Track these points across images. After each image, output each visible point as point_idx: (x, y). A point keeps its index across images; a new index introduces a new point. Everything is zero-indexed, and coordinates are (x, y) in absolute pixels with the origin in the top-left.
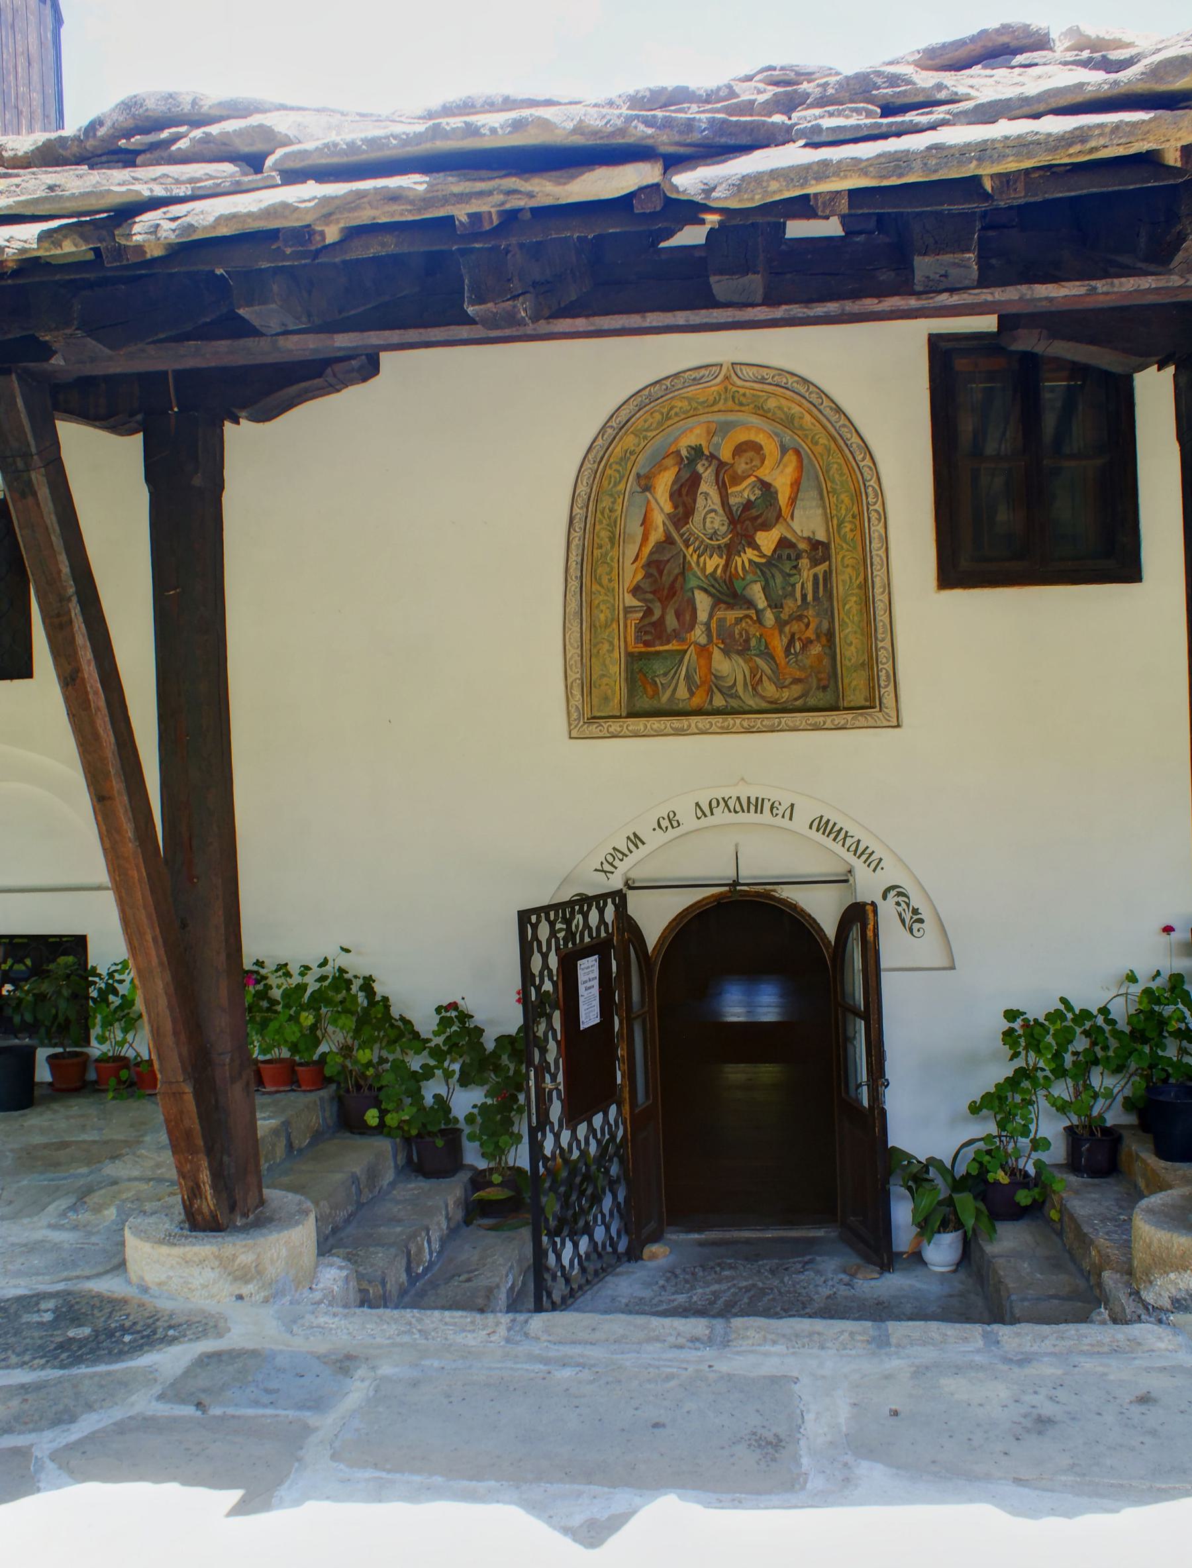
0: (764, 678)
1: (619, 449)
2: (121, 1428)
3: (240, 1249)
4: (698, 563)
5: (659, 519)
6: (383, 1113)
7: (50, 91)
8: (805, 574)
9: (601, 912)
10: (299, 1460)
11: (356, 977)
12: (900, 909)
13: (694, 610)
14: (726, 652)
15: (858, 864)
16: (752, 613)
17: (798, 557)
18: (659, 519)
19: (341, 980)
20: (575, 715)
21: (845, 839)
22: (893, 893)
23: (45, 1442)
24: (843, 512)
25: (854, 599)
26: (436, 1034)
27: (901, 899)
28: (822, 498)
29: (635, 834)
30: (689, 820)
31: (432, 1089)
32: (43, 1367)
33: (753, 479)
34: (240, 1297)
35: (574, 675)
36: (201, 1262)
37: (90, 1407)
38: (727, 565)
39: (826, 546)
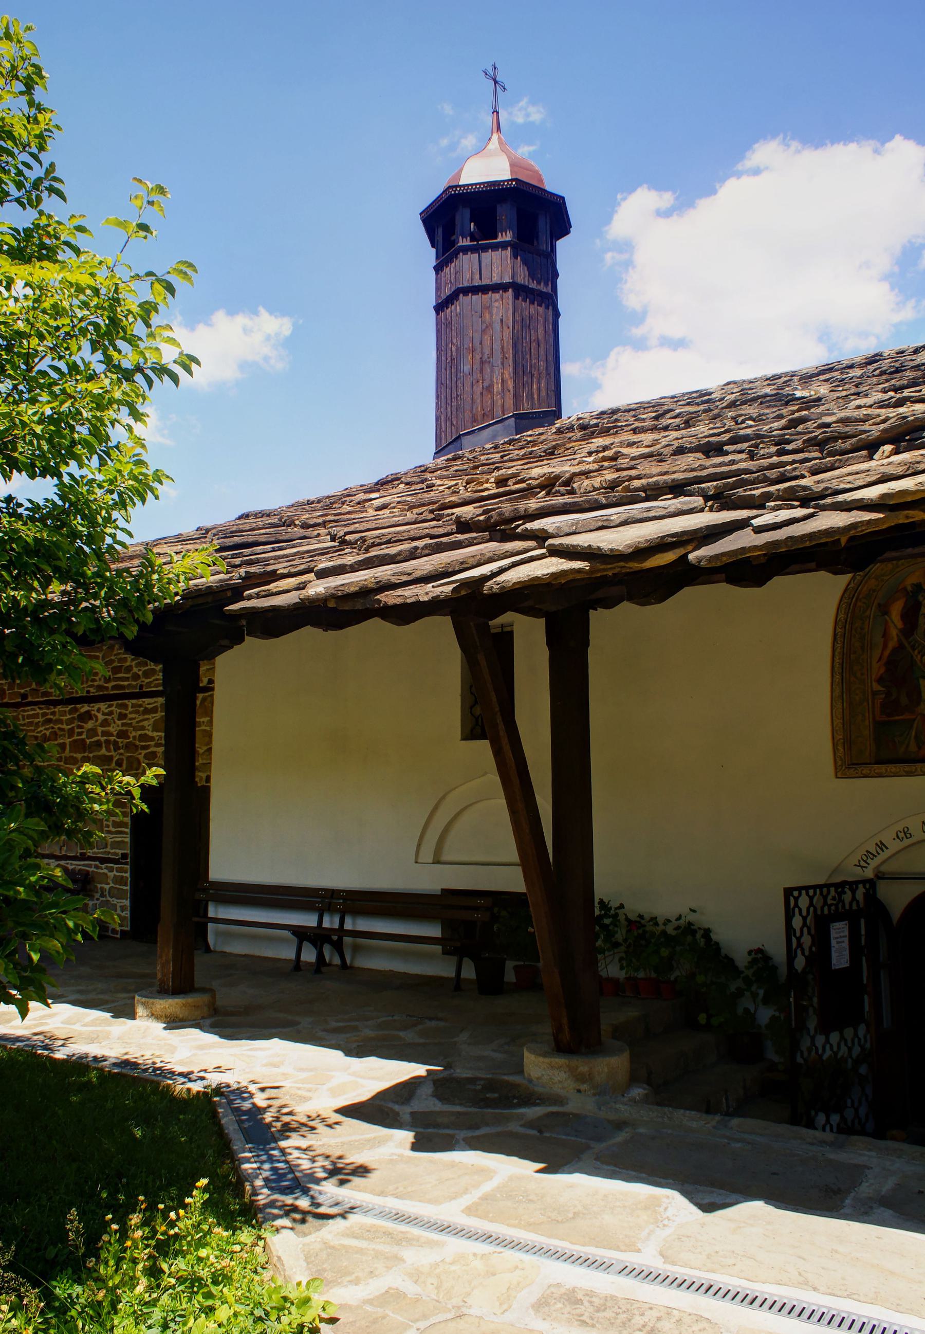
3: (582, 1065)
5: (894, 633)
7: (551, 358)
11: (700, 928)
18: (894, 633)
19: (689, 929)
20: (839, 763)
23: (462, 1134)
26: (747, 968)
31: (746, 1003)
32: (470, 1107)
34: (579, 1091)
35: (839, 737)
37: (487, 1125)
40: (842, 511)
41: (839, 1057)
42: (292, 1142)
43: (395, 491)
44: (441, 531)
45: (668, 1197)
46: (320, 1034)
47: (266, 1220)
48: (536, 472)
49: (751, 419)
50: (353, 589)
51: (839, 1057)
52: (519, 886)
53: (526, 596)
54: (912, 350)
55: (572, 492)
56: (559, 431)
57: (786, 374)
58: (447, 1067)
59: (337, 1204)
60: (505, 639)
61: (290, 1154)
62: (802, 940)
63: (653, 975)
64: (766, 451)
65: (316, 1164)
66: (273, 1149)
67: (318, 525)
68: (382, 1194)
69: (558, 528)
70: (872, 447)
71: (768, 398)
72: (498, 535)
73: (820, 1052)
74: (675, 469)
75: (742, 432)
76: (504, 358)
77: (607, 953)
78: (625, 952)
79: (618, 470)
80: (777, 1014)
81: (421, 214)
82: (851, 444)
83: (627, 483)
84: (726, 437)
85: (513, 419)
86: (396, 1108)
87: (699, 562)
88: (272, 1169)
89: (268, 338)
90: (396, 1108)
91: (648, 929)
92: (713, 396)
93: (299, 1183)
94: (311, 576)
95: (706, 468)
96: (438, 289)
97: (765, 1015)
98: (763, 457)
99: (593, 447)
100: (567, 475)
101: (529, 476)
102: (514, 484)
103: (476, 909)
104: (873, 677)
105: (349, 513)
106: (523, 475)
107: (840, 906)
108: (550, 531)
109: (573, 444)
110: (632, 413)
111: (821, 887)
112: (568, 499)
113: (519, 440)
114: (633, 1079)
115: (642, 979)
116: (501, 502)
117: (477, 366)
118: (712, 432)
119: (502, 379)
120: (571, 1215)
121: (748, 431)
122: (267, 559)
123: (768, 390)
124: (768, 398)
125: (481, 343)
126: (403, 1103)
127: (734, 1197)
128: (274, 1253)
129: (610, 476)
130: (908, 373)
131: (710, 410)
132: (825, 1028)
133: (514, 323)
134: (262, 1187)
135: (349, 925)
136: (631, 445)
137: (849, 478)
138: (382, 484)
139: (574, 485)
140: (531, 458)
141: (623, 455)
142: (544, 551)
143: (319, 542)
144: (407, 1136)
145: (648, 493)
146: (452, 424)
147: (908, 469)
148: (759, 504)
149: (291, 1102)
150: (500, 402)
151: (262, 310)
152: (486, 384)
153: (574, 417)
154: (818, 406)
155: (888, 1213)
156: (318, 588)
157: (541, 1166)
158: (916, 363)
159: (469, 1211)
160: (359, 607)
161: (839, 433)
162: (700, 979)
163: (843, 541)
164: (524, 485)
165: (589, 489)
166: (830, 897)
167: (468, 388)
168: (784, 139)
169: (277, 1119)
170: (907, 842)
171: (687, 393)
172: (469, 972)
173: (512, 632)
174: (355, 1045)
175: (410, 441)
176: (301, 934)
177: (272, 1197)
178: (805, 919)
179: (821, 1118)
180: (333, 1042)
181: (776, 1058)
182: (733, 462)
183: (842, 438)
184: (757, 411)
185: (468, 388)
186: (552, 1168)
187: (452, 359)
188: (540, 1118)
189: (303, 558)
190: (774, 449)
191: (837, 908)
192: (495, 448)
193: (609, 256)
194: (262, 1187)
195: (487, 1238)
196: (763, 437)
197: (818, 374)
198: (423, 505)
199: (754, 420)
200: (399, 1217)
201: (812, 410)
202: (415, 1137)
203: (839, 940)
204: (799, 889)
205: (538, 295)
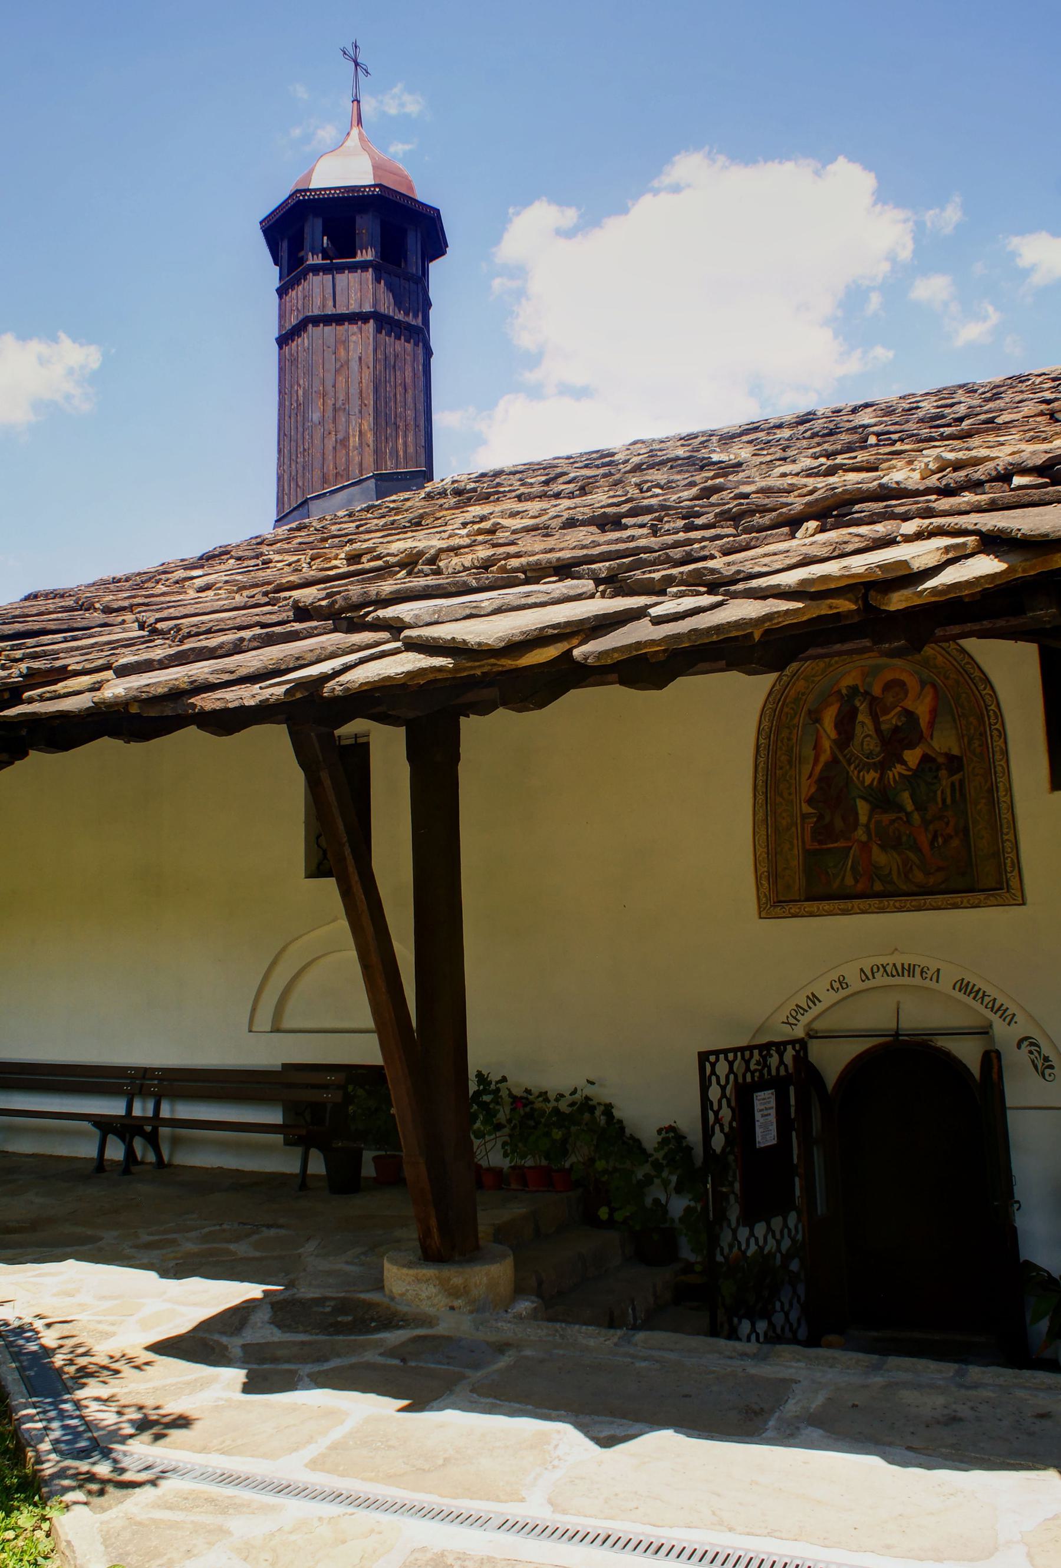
0: (914, 867)
1: (793, 691)
2: (352, 1367)
3: (456, 1275)
4: (858, 778)
5: (827, 744)
6: (612, 1211)
7: (421, 408)
8: (944, 782)
9: (781, 1056)
10: (451, 1391)
11: (599, 1104)
12: (1032, 1056)
13: (857, 814)
14: (883, 847)
15: (995, 1018)
16: (902, 815)
17: (938, 769)
18: (827, 744)
19: (587, 1105)
21: (982, 998)
22: (1026, 1043)
23: (309, 1368)
24: (972, 731)
25: (984, 801)
26: (656, 1150)
27: (1033, 1048)
28: (954, 721)
29: (813, 994)
30: (945, 985)
31: (656, 1192)
32: (317, 1334)
33: (899, 709)
35: (761, 869)
36: (427, 1280)
38: (881, 779)
39: (959, 759)
40: (756, 598)
41: (766, 1252)
42: (92, 1389)
43: (223, 567)
44: (274, 618)
45: (559, 1432)
46: (129, 1251)
47: (52, 1494)
48: (395, 547)
49: (658, 486)
50: (160, 690)
51: (766, 1252)
52: (378, 1060)
53: (377, 701)
54: (849, 409)
55: (438, 572)
56: (429, 497)
57: (704, 433)
58: (289, 1285)
59: (147, 1468)
60: (360, 751)
61: (87, 1407)
62: (721, 1114)
63: (544, 1163)
64: (672, 525)
65: (125, 1418)
66: (65, 1402)
67: (124, 609)
68: (204, 1450)
69: (417, 616)
70: (794, 523)
71: (680, 462)
72: (344, 624)
73: (743, 1247)
74: (562, 545)
75: (646, 502)
76: (363, 405)
77: (487, 1138)
78: (510, 1136)
79: (494, 546)
80: (692, 1204)
81: (261, 223)
82: (770, 519)
83: (503, 562)
84: (626, 507)
85: (373, 480)
86: (224, 1340)
87: (586, 659)
88: (64, 1427)
89: (71, 371)
90: (224, 1340)
91: (537, 1105)
92: (616, 457)
93: (98, 1444)
94: (109, 674)
95: (599, 545)
96: (282, 316)
97: (678, 1206)
98: (668, 532)
99: (468, 517)
100: (433, 551)
101: (386, 551)
102: (369, 561)
103: (325, 1087)
104: (803, 797)
105: (163, 594)
106: (382, 550)
107: (765, 1071)
108: (407, 620)
109: (445, 513)
110: (518, 476)
111: (742, 1049)
112: (431, 581)
113: (379, 507)
114: (519, 1290)
115: (530, 1168)
116: (351, 583)
117: (329, 413)
118: (611, 501)
119: (360, 431)
120: (441, 1462)
121: (654, 501)
122: (57, 652)
123: (681, 452)
124: (680, 462)
125: (334, 386)
126: (232, 1334)
127: (638, 1426)
128: (63, 1537)
129: (483, 553)
130: (843, 436)
131: (611, 474)
132: (749, 1219)
133: (375, 361)
134: (49, 1452)
135: (165, 1112)
136: (513, 515)
137: (766, 560)
138: (208, 559)
139: (441, 564)
140: (393, 529)
141: (503, 527)
142: (399, 644)
143: (125, 631)
144: (236, 1375)
145: (529, 574)
146: (297, 485)
147: (834, 550)
148: (659, 589)
149: (90, 1340)
150: (357, 459)
151: (63, 336)
152: (340, 436)
153: (448, 480)
154: (738, 472)
155: (816, 1433)
156: (116, 689)
157: (406, 1402)
158: (853, 424)
159: (314, 1465)
160: (168, 712)
161: (757, 506)
162: (600, 1165)
163: (757, 635)
164: (380, 563)
165: (458, 568)
166: (753, 1061)
167: (317, 441)
168: (710, 152)
169: (71, 1362)
170: (843, 993)
171: (586, 453)
172: (317, 1166)
173: (368, 744)
174: (172, 1264)
175: (242, 506)
176: (105, 1125)
177: (63, 1464)
178: (723, 1088)
179: (745, 1327)
180: (145, 1261)
181: (692, 1258)
182: (632, 538)
183: (760, 512)
184: (665, 476)
185: (317, 441)
186: (417, 1405)
187: (299, 405)
188: (403, 1344)
189: (102, 651)
190: (681, 523)
191: (762, 1075)
192: (350, 515)
193: (497, 283)
194: (49, 1452)
195: (337, 1497)
196: (670, 508)
197: (741, 434)
198: (256, 586)
199: (662, 488)
200: (226, 1479)
201: (730, 478)
202: (247, 1376)
203: (766, 1112)
204: (717, 1053)
205: (405, 329)
